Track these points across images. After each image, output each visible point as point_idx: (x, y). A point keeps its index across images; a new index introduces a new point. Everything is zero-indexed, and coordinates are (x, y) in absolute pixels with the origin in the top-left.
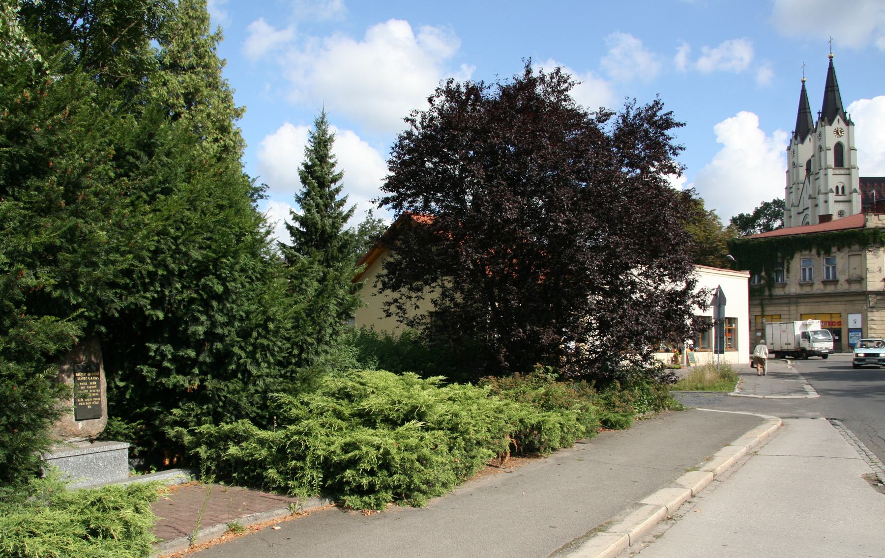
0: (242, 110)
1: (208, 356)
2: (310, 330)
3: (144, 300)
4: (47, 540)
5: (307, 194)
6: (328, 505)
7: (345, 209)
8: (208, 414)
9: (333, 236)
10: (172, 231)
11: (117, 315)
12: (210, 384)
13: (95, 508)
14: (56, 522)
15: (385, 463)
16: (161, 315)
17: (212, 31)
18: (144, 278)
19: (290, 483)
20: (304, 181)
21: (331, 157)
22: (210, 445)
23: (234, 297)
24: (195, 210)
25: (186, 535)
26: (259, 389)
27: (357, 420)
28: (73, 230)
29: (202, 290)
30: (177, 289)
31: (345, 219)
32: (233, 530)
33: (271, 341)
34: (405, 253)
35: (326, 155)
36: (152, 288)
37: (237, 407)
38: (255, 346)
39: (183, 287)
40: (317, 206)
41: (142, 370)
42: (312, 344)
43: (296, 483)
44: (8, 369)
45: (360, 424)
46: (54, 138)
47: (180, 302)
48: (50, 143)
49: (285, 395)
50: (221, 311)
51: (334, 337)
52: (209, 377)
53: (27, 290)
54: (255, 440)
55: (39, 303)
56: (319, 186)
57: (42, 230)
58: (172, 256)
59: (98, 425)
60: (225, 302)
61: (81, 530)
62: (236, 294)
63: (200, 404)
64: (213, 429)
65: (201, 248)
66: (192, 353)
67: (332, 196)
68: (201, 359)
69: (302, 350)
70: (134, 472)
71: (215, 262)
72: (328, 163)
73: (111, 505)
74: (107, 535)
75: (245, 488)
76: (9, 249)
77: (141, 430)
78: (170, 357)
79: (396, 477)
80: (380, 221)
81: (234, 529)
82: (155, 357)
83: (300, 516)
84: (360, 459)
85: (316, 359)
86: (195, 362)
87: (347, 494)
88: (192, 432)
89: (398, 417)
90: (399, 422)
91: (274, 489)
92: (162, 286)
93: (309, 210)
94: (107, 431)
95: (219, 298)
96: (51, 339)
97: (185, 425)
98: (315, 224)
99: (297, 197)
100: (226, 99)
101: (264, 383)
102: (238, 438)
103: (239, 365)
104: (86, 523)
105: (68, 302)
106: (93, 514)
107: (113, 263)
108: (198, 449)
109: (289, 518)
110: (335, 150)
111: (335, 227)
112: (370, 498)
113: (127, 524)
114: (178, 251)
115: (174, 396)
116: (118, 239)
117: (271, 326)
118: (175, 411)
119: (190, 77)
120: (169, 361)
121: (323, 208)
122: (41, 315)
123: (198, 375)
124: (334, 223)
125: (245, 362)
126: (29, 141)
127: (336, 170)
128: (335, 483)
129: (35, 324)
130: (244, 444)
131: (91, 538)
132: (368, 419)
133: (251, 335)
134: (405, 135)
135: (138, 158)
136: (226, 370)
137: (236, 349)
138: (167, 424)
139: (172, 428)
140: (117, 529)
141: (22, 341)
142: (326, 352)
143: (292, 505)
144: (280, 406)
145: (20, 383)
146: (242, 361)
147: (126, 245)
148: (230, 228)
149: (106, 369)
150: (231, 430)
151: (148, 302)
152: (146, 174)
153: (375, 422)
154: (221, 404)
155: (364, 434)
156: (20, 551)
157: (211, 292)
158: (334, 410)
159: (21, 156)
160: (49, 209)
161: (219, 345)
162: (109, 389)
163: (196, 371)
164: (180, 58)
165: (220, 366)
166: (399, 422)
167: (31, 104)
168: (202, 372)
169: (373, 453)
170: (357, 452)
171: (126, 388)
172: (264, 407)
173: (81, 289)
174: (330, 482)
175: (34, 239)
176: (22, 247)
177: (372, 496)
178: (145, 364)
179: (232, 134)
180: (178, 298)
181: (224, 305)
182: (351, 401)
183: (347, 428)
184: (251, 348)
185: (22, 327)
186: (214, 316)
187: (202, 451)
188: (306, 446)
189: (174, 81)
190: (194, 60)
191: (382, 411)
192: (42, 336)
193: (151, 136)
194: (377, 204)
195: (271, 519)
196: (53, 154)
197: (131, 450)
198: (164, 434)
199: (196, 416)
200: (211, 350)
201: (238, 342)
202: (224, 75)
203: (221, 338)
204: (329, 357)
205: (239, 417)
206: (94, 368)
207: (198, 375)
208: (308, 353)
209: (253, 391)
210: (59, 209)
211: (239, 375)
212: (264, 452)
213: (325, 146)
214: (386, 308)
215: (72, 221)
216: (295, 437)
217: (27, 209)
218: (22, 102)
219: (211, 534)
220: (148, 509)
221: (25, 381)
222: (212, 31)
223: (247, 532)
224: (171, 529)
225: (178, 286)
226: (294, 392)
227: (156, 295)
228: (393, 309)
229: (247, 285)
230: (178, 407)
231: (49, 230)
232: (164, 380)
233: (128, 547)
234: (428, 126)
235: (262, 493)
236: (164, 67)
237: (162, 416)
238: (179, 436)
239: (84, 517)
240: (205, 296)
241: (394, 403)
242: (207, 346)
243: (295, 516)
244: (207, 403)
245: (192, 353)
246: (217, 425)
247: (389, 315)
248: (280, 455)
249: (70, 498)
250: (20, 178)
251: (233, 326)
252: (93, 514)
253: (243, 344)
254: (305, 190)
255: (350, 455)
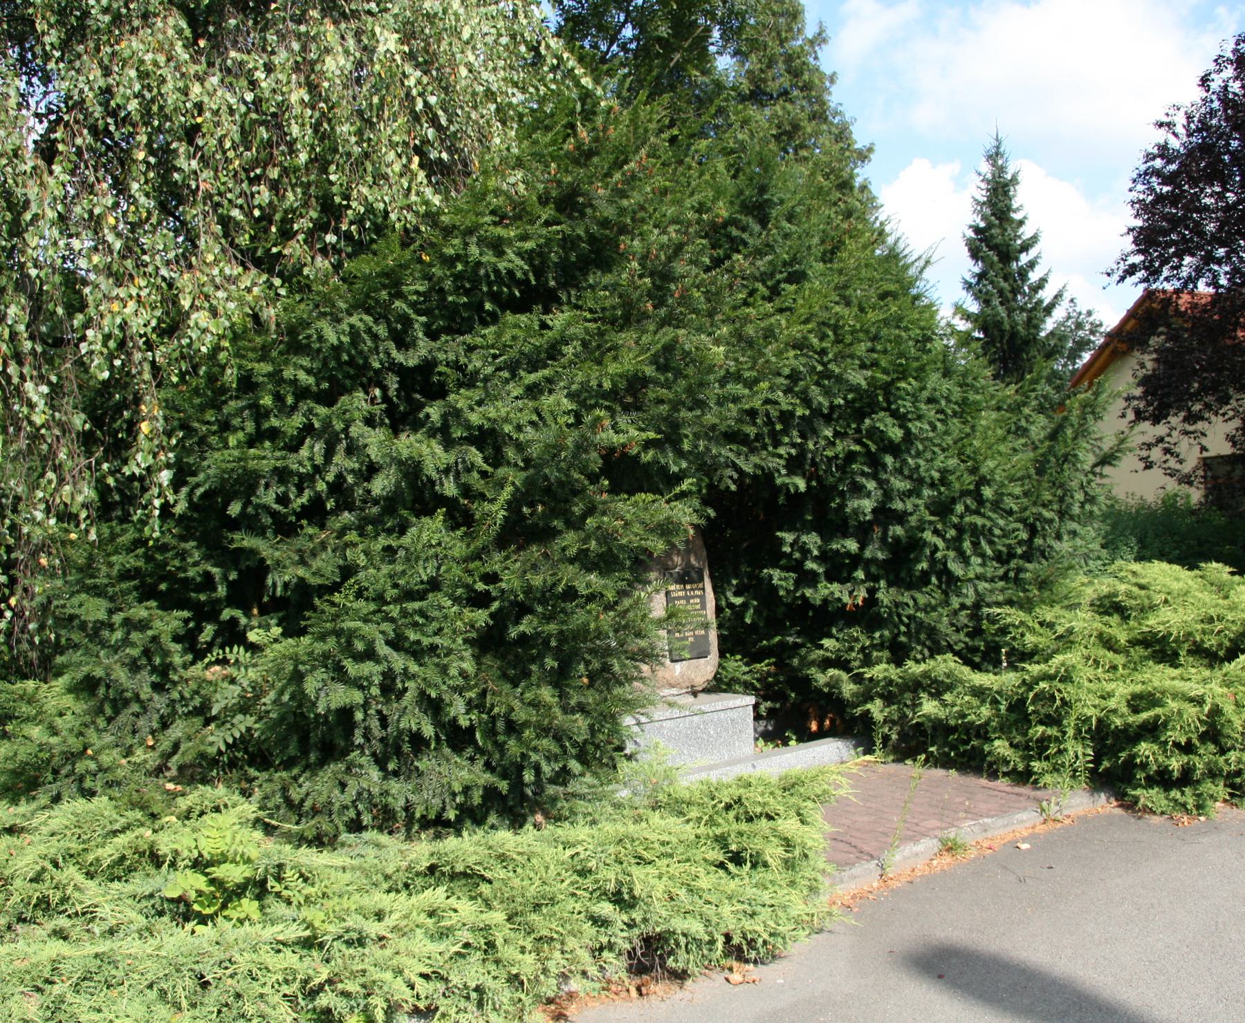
0: (870, 150)
1: (880, 549)
2: (1047, 496)
3: (774, 461)
4: (664, 869)
5: (981, 276)
6: (1104, 804)
7: (1046, 295)
8: (881, 647)
9: (1031, 340)
10: (815, 341)
11: (733, 487)
12: (886, 596)
13: (732, 814)
14: (674, 840)
15: (1213, 732)
16: (802, 484)
17: (810, 32)
18: (773, 424)
19: (1036, 765)
20: (975, 254)
21: (1018, 210)
22: (889, 699)
23: (921, 447)
24: (848, 304)
25: (872, 857)
26: (969, 602)
27: (1140, 651)
28: (669, 348)
29: (869, 437)
30: (826, 438)
31: (1048, 310)
32: (950, 849)
33: (989, 518)
34: (1181, 354)
35: (1009, 208)
36: (786, 440)
37: (932, 631)
38: (960, 529)
39: (837, 434)
40: (1001, 292)
41: (771, 577)
42: (1051, 521)
43: (1045, 764)
44: (588, 585)
45: (1147, 658)
46: (625, 203)
47: (830, 459)
48: (622, 211)
49: (1013, 611)
50: (899, 471)
51: (1088, 507)
52: (882, 583)
53: (609, 454)
54: (969, 691)
55: (625, 473)
56: (1001, 261)
57: (623, 351)
58: (817, 384)
59: (706, 669)
60: (906, 456)
61: (717, 855)
62: (922, 441)
63: (870, 629)
64: (893, 672)
65: (863, 366)
66: (852, 545)
67: (1023, 274)
68: (868, 554)
69: (1033, 531)
70: (761, 742)
71: (887, 388)
72: (1011, 221)
73: (759, 810)
74: (758, 862)
75: (953, 772)
76: (574, 387)
77: (769, 674)
78: (816, 553)
79: (1233, 756)
80: (1089, 313)
81: (950, 848)
82: (791, 554)
83: (1059, 825)
84: (1165, 724)
85: (1057, 545)
86: (857, 560)
87: (1140, 786)
88: (858, 679)
89: (1220, 645)
90: (1221, 653)
91: (1005, 774)
92: (803, 436)
93: (987, 302)
94: (717, 678)
95: (894, 449)
96: (652, 531)
97: (844, 665)
98: (998, 325)
99: (966, 282)
100: (842, 135)
101: (976, 590)
102: (938, 688)
103: (932, 560)
104: (722, 841)
105: (664, 469)
106: (728, 825)
107: (736, 400)
108: (869, 706)
109: (1041, 829)
110: (1024, 200)
111: (1033, 324)
112: (1183, 793)
113: (788, 844)
114: (827, 374)
115: (824, 619)
116: (736, 360)
117: (988, 492)
118: (827, 642)
119: (784, 108)
120: (815, 559)
121: (1010, 296)
122: (631, 493)
123: (863, 582)
124: (1030, 319)
125: (945, 557)
126: (589, 211)
127: (1026, 232)
128: (1117, 765)
129: (625, 506)
130: (948, 697)
131: (731, 866)
132: (1161, 649)
133: (952, 511)
134: (1155, 151)
135: (744, 229)
136: (910, 571)
137: (928, 536)
138: (812, 663)
139: (824, 671)
140: (773, 853)
141: (606, 537)
142: (1074, 533)
143: (1044, 804)
144: (1004, 631)
145: (609, 607)
146: (939, 555)
147: (752, 369)
148: (906, 329)
149: (712, 577)
150: (926, 674)
151: (782, 462)
152: (759, 253)
153: (1176, 655)
154: (903, 629)
155: (1159, 677)
156: (625, 890)
157: (882, 440)
158: (1100, 636)
159: (579, 237)
160: (628, 317)
161: (898, 530)
162: (719, 610)
163: (860, 574)
164: (765, 81)
165: (901, 564)
166: (1221, 653)
167: (590, 150)
168: (871, 577)
169: (1191, 711)
170: (1158, 711)
171: (745, 606)
172: (977, 632)
173: (686, 446)
174: (1106, 764)
175: (613, 368)
176: (594, 383)
177: (1187, 790)
178: (775, 565)
179: (856, 191)
180: (830, 453)
181: (904, 462)
182: (1125, 618)
183: (1124, 666)
184: (952, 533)
185: (604, 513)
186: (888, 481)
187: (877, 709)
188: (1062, 699)
189: (761, 117)
190: (785, 81)
191: (1190, 634)
192: (637, 528)
193: (763, 189)
194: (1116, 277)
195: (1009, 829)
196: (623, 230)
197: (756, 707)
198: (808, 680)
199: (863, 649)
200: (883, 540)
201: (931, 523)
202: (836, 97)
203: (901, 518)
204: (1079, 542)
205: (936, 650)
206: (694, 575)
207: (863, 582)
208: (1044, 538)
209: (957, 606)
210: (645, 315)
211: (934, 580)
212: (986, 711)
213: (1006, 193)
214: (1144, 453)
215: (667, 334)
216: (1043, 685)
217: (595, 320)
218: (578, 148)
219: (913, 857)
220: (816, 814)
221: (616, 603)
222: (810, 32)
223: (973, 853)
224: (850, 849)
225: (828, 433)
226: (1027, 605)
227: (793, 451)
228: (1156, 454)
229: (939, 424)
230: (830, 636)
231: (631, 354)
232: (808, 593)
233: (792, 884)
234: (1199, 130)
235: (983, 781)
236: (743, 98)
237: (803, 651)
238: (834, 684)
239: (718, 831)
240: (873, 448)
241: (1211, 620)
242: (877, 532)
243: (1050, 825)
244: (880, 628)
245: (852, 545)
246: (899, 664)
247: (1149, 466)
248: (1013, 716)
249: (686, 795)
250: (578, 273)
251: (919, 496)
252: (728, 825)
253: (939, 526)
254: (977, 270)
255: (1145, 716)
